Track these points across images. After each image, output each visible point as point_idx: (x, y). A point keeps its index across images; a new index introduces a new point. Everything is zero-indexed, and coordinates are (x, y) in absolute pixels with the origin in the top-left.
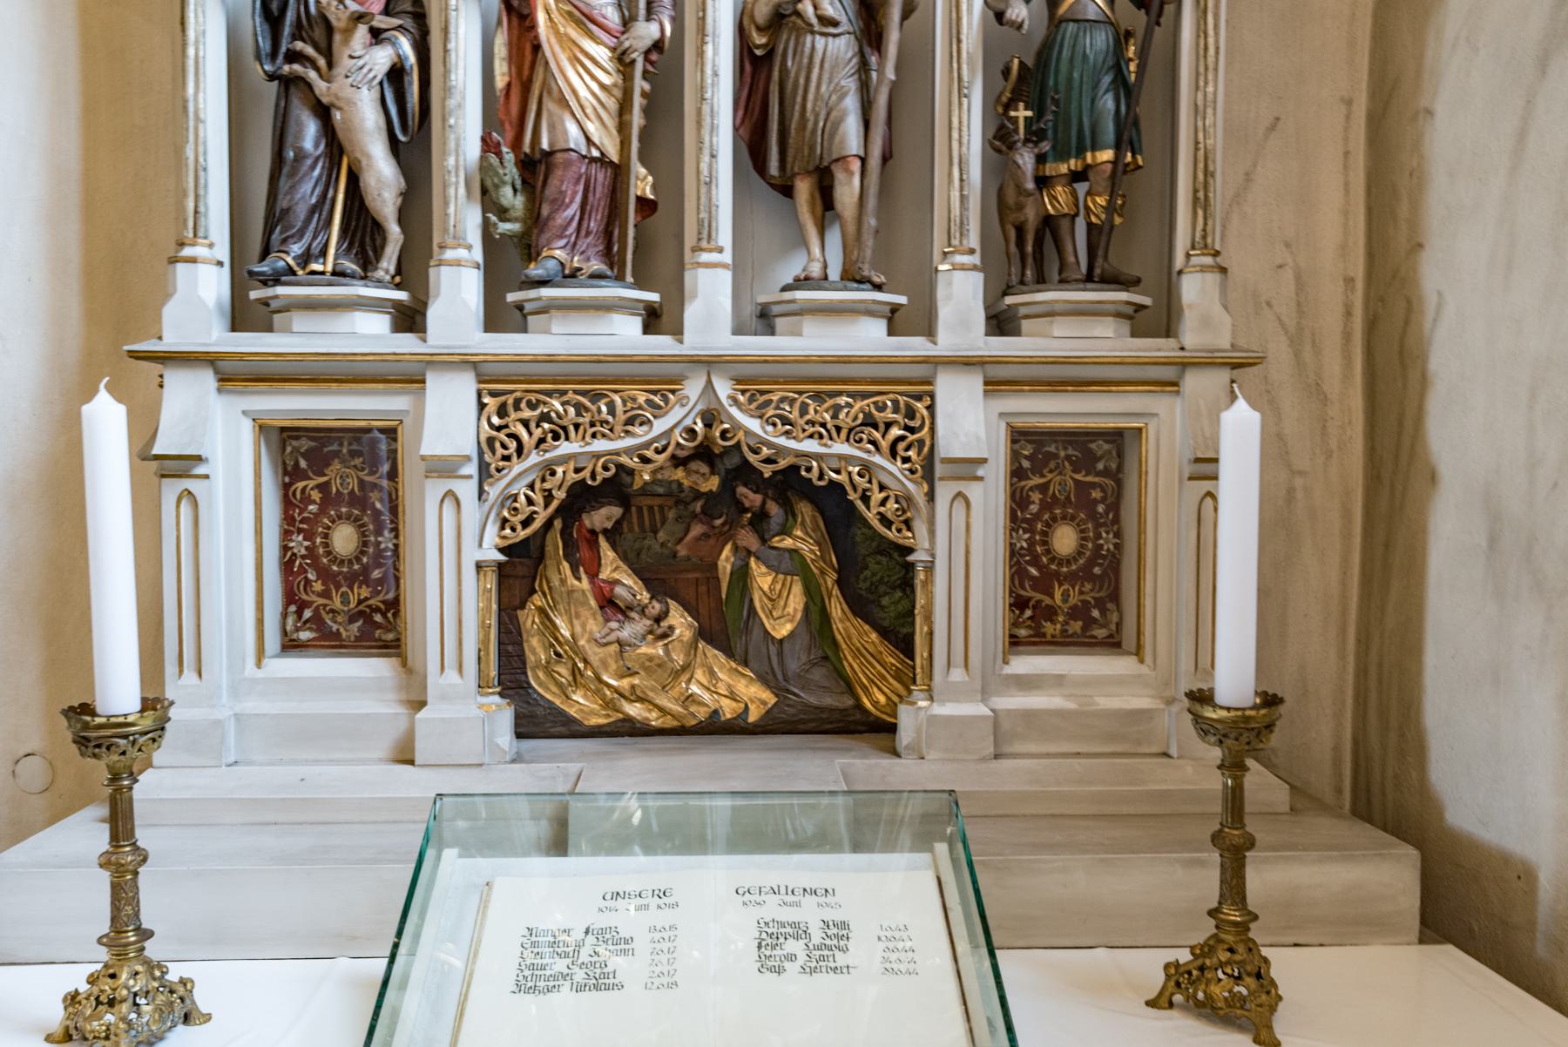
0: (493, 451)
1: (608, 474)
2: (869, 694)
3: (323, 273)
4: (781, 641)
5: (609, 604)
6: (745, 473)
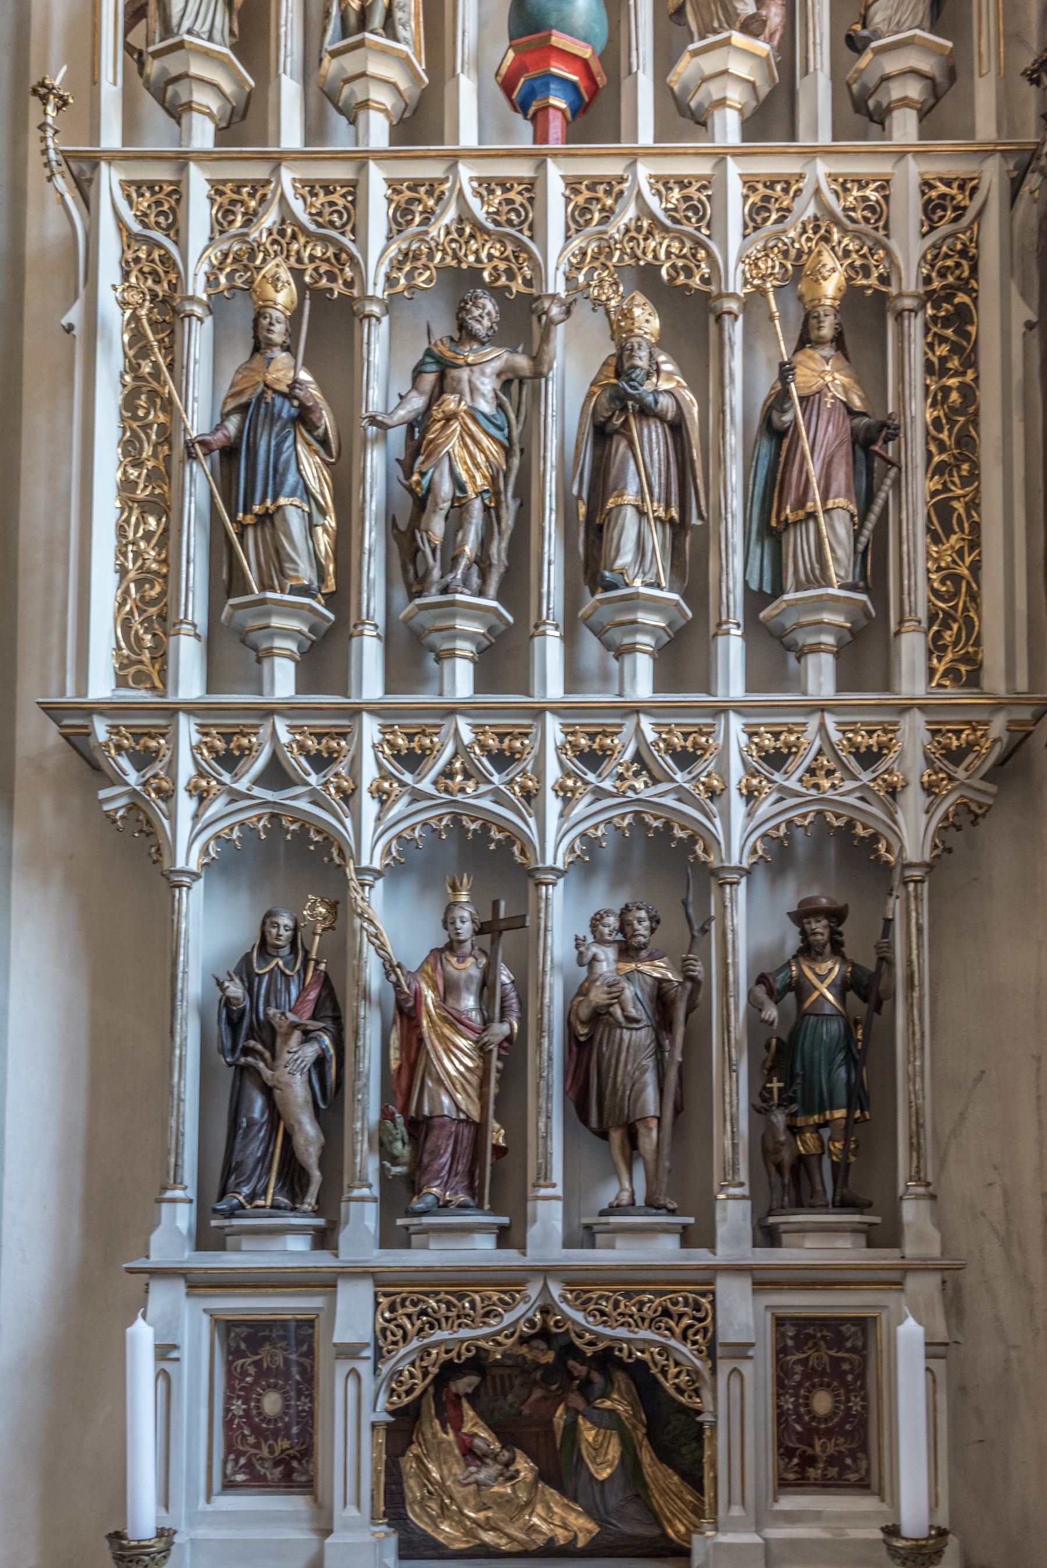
0: (385, 1338)
2: (672, 1526)
3: (264, 1207)
4: (603, 1482)
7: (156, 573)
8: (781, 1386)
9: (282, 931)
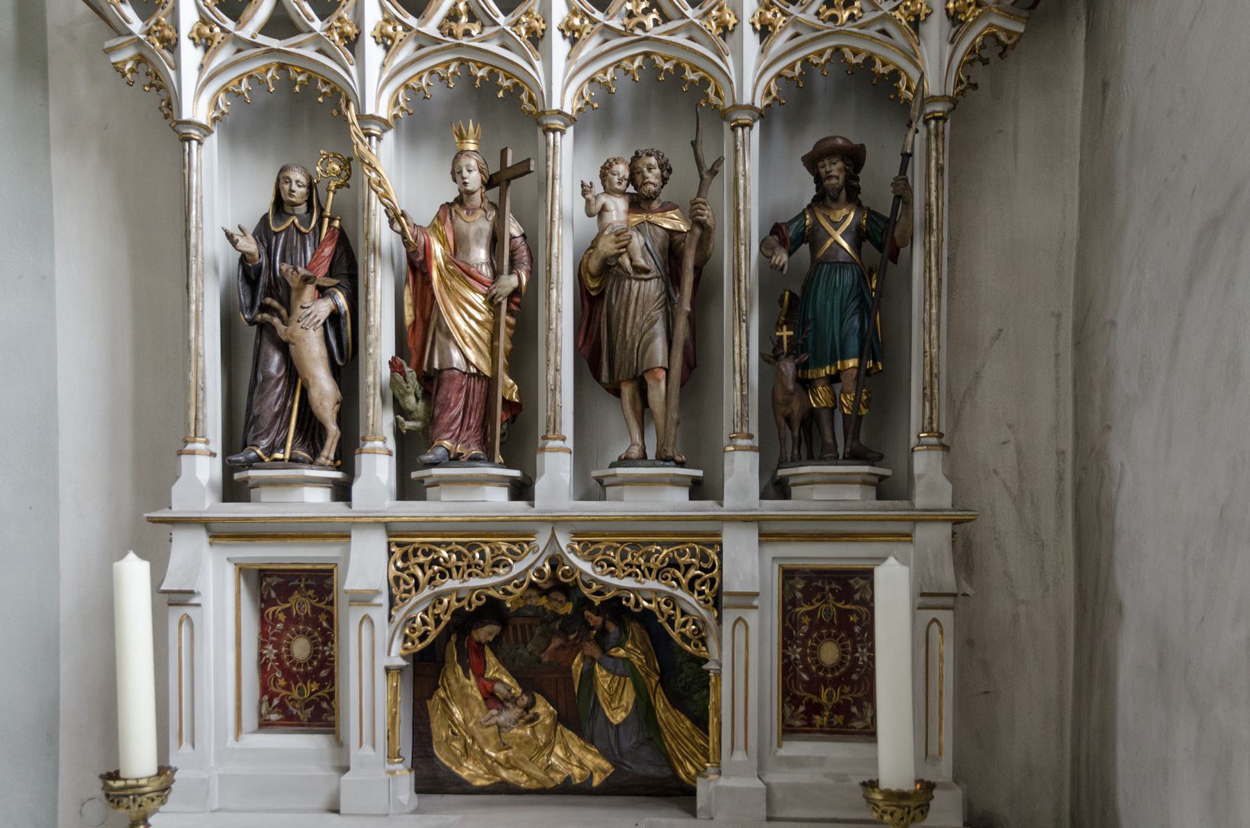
0: (398, 585)
1: (480, 603)
2: (684, 768)
3: (283, 460)
4: (618, 726)
5: (491, 698)
6: (586, 602)
8: (788, 635)
9: (294, 187)
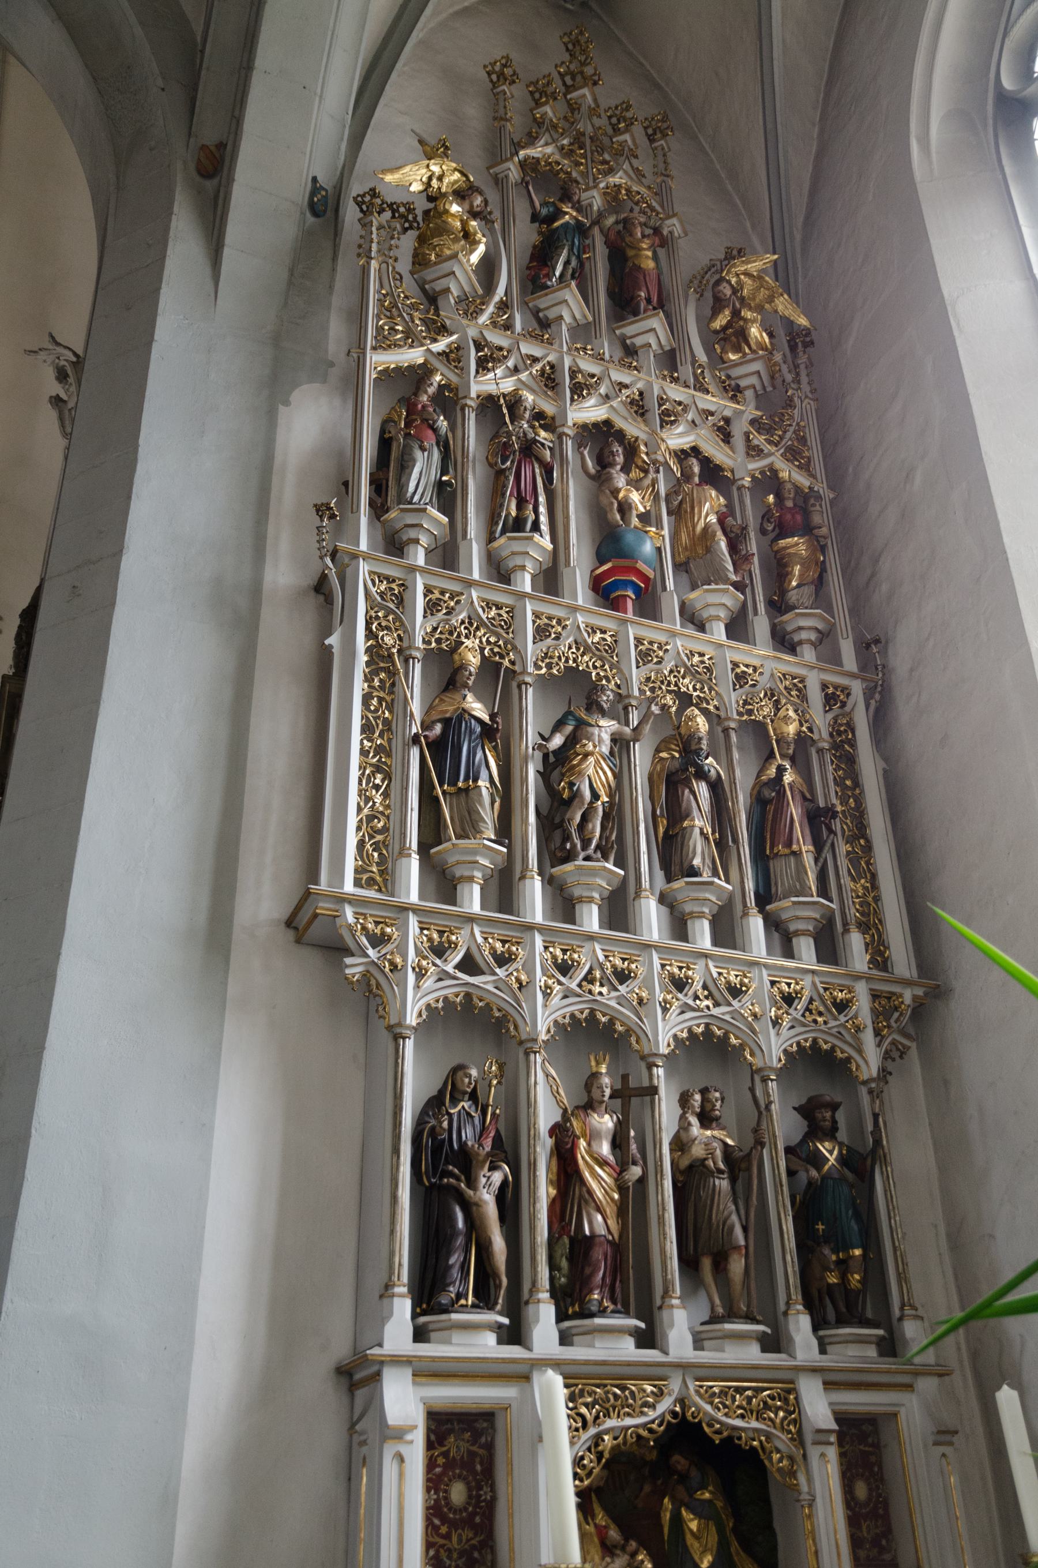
3: (467, 1306)
7: (382, 813)
